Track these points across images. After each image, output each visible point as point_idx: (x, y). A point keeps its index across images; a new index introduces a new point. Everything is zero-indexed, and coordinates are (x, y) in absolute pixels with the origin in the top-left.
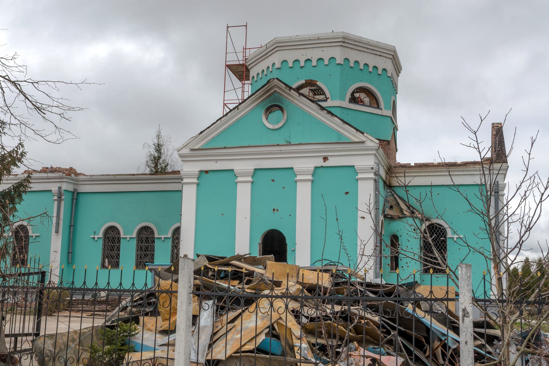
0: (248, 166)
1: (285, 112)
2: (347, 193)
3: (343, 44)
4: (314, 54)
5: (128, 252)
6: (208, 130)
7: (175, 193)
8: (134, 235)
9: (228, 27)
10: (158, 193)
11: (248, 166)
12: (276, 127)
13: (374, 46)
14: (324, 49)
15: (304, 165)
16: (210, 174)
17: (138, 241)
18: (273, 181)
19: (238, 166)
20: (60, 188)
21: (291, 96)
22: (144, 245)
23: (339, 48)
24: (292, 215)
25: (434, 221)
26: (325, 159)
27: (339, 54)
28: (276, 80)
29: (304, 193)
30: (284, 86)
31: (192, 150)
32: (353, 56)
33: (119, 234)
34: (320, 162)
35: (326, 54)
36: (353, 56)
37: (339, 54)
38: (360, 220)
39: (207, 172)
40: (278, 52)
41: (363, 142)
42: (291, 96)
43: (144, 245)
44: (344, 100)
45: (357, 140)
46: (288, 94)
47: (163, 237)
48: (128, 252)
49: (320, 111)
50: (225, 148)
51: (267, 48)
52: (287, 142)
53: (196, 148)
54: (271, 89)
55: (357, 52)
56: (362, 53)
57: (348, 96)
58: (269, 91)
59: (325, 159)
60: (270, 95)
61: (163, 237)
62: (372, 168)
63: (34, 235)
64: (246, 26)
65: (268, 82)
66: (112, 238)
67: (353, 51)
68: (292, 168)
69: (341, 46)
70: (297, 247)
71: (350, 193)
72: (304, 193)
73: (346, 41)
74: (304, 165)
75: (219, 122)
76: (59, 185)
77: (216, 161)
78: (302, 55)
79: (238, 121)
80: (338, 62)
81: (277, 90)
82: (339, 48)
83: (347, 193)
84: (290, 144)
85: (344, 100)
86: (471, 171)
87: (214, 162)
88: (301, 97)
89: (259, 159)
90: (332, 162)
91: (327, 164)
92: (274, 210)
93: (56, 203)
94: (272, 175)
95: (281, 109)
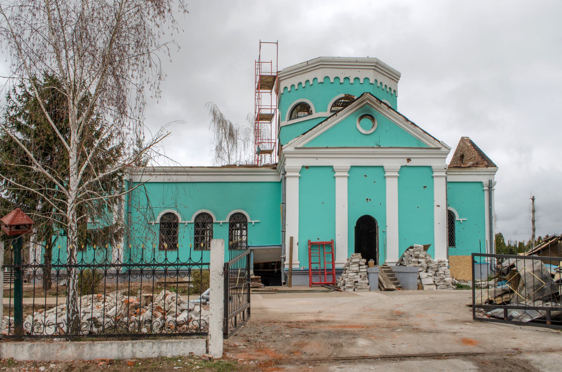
0: (346, 163)
1: (376, 121)
2: (425, 187)
4: (352, 74)
5: (186, 236)
6: (310, 132)
7: (231, 184)
8: (193, 221)
9: (260, 43)
10: (214, 184)
11: (346, 163)
12: (368, 132)
13: (391, 72)
14: (360, 70)
15: (393, 164)
16: (310, 169)
17: (195, 225)
18: (366, 176)
19: (337, 163)
21: (381, 108)
22: (200, 229)
23: (372, 71)
24: (383, 204)
26: (409, 160)
28: (368, 94)
29: (392, 187)
30: (375, 99)
31: (296, 148)
33: (247, 220)
34: (405, 163)
38: (436, 208)
39: (307, 167)
40: (321, 69)
41: (439, 148)
42: (381, 108)
43: (200, 229)
45: (433, 147)
46: (378, 106)
47: (221, 222)
48: (186, 236)
49: (405, 122)
50: (327, 148)
51: (308, 65)
52: (377, 145)
53: (299, 146)
54: (364, 101)
56: (384, 76)
58: (362, 102)
59: (409, 160)
60: (362, 106)
61: (221, 222)
62: (445, 168)
64: (277, 43)
65: (362, 95)
66: (169, 226)
68: (382, 167)
69: (374, 69)
70: (388, 229)
71: (428, 188)
72: (392, 187)
73: (377, 66)
74: (393, 164)
75: (320, 125)
77: (317, 158)
78: (342, 74)
79: (335, 126)
81: (369, 102)
82: (372, 71)
83: (425, 187)
84: (379, 147)
86: (473, 172)
87: (315, 159)
88: (390, 109)
89: (354, 158)
90: (413, 163)
91: (410, 164)
92: (367, 199)
93: (486, 193)
94: (366, 172)
95: (372, 118)
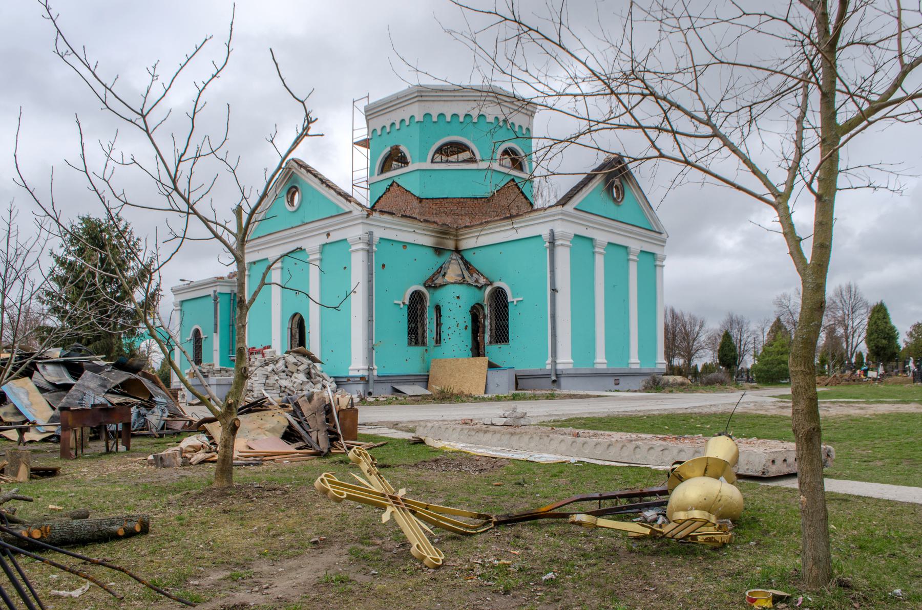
3: (420, 99)
14: (405, 108)
15: (312, 245)
20: (215, 292)
23: (417, 104)
25: (497, 284)
26: (328, 235)
27: (416, 111)
32: (435, 109)
34: (324, 239)
35: (405, 113)
36: (435, 109)
37: (416, 111)
39: (254, 263)
41: (350, 212)
44: (425, 161)
55: (442, 103)
56: (449, 103)
57: (429, 159)
63: (515, 300)
67: (436, 103)
76: (215, 289)
77: (587, 227)
80: (488, 121)
85: (425, 161)
